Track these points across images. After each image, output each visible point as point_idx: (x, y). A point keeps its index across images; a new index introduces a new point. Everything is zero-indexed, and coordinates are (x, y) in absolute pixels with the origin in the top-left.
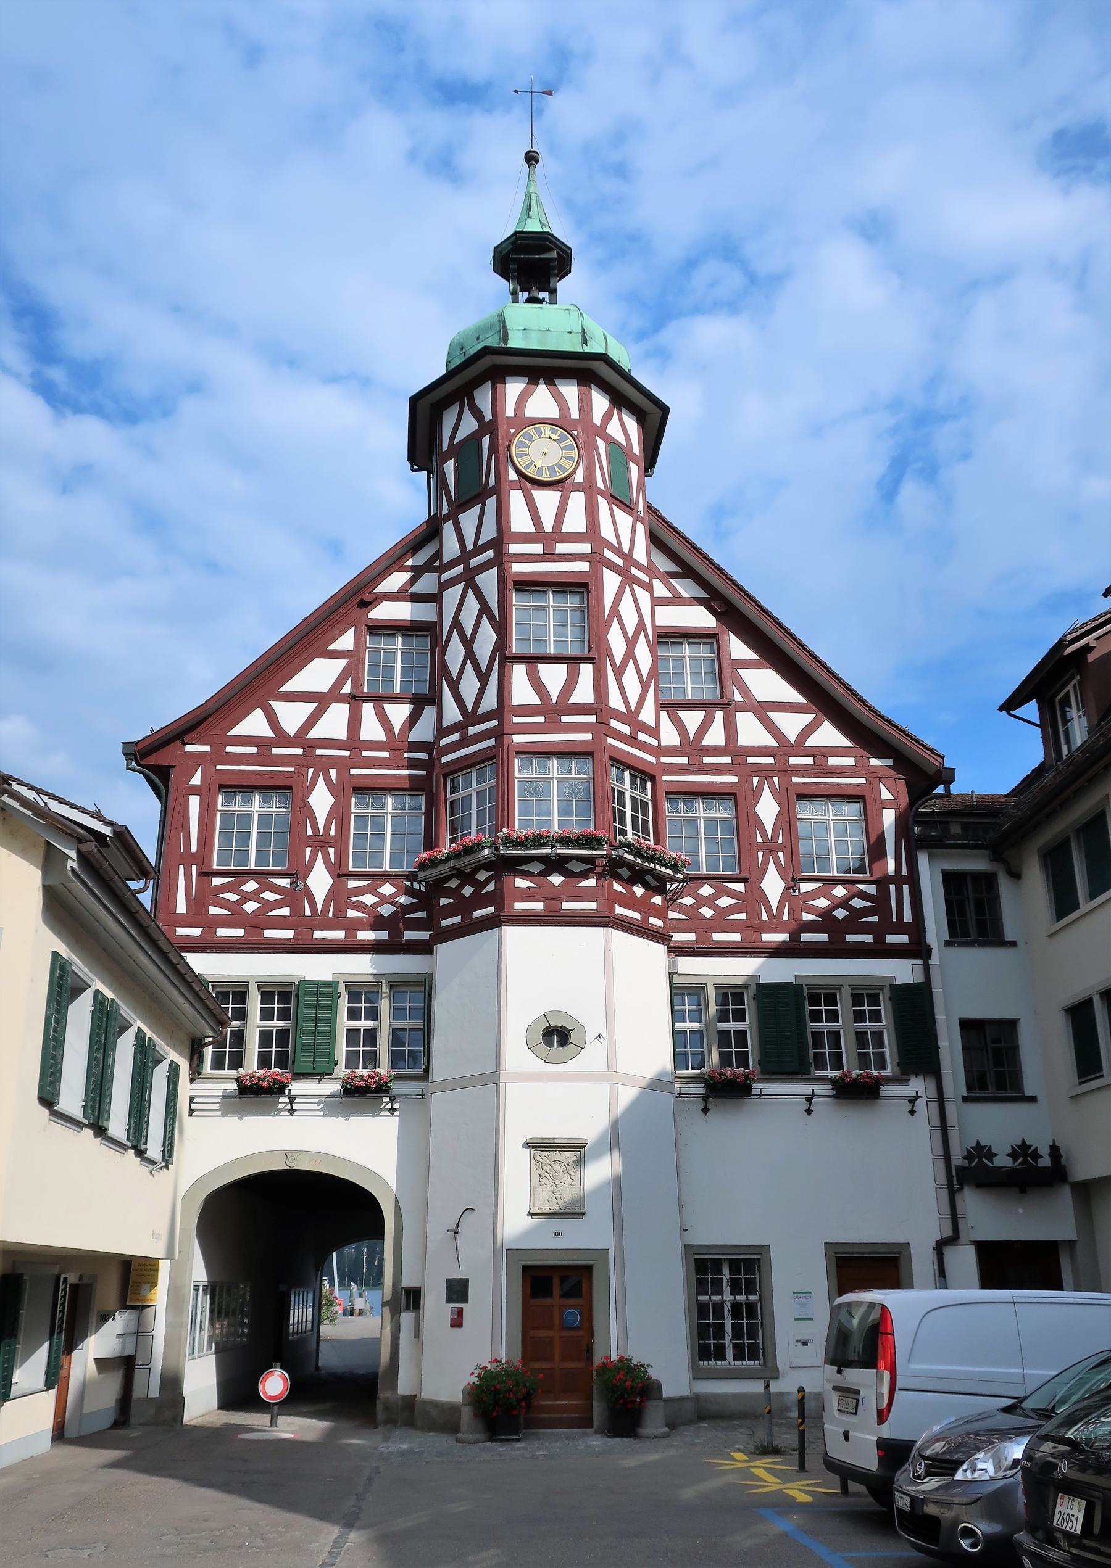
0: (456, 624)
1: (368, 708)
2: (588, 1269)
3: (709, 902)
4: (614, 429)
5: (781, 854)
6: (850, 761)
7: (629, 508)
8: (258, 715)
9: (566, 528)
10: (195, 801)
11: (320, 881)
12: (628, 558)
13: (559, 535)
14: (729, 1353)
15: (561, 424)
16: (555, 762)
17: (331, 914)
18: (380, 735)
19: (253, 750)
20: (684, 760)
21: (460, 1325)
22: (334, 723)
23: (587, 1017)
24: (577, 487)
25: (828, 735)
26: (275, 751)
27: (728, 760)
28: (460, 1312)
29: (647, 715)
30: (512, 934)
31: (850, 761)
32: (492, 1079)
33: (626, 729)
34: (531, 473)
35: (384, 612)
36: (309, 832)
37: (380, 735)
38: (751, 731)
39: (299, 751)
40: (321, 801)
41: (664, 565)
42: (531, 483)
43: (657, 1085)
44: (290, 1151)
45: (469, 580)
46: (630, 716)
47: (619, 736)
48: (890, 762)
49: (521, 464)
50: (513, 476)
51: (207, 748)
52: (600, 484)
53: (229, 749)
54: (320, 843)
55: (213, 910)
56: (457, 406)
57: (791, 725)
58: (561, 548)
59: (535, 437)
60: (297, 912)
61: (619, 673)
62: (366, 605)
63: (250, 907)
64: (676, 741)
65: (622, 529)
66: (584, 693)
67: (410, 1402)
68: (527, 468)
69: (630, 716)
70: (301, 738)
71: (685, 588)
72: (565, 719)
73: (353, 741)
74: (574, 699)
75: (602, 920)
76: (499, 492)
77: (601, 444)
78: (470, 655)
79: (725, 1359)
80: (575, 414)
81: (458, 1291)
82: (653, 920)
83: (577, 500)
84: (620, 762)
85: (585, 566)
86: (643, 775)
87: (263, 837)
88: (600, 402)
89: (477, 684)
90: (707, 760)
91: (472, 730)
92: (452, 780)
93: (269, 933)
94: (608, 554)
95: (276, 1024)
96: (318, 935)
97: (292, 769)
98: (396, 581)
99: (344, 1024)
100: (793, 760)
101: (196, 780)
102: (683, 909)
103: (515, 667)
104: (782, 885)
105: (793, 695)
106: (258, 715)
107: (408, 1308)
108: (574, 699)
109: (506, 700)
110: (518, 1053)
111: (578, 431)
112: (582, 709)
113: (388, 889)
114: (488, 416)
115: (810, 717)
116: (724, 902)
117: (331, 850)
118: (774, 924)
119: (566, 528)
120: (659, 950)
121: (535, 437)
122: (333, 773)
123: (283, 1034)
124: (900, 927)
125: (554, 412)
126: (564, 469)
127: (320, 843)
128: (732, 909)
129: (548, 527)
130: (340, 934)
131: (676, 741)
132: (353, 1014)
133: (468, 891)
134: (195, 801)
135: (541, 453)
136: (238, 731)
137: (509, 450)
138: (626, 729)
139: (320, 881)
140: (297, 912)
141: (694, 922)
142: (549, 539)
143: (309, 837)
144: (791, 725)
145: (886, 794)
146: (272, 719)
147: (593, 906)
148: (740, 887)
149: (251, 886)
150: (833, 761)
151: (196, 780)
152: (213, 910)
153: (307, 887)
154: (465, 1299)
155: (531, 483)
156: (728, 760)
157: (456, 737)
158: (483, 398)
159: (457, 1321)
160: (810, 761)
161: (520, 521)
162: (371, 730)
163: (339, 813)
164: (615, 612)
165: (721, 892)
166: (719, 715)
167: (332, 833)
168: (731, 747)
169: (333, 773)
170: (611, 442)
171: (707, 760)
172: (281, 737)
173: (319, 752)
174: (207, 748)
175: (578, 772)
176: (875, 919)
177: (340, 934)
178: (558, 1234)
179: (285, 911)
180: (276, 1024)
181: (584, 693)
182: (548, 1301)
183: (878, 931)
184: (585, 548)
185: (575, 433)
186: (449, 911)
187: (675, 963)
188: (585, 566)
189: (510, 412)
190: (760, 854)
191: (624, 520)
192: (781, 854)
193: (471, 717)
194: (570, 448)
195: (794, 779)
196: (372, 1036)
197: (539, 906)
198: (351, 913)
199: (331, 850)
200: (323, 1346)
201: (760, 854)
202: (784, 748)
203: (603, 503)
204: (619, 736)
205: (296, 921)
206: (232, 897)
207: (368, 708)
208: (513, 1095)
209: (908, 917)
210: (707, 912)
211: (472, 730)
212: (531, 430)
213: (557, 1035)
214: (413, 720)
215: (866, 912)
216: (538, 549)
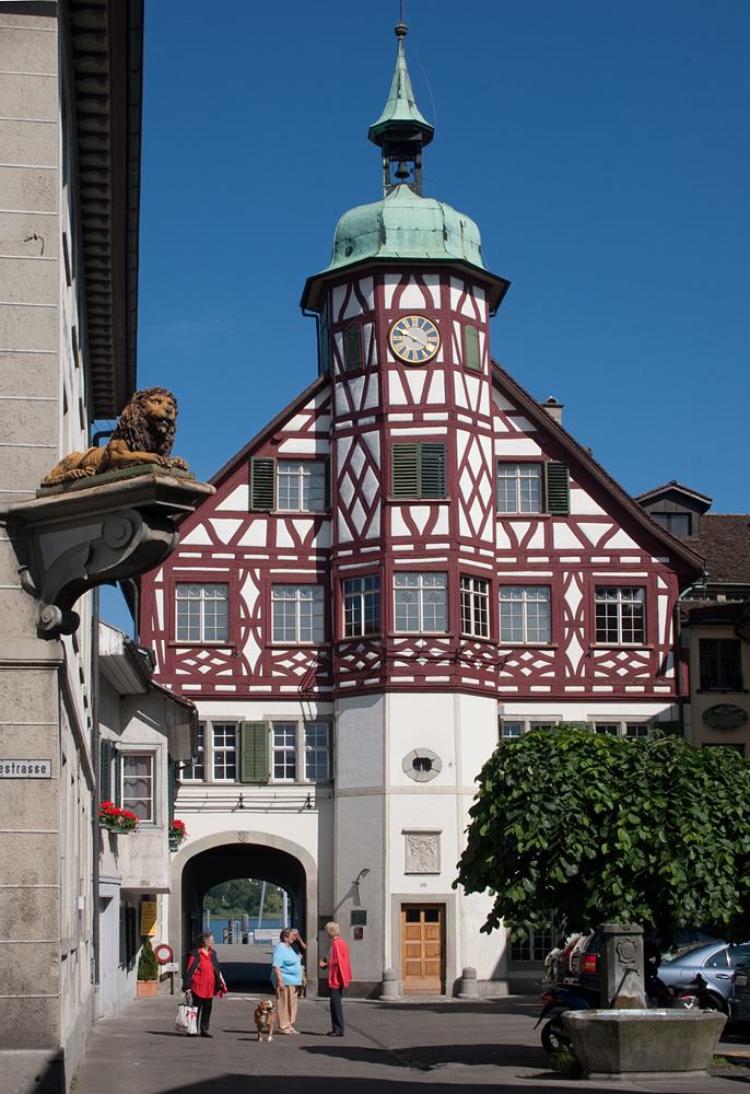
0: (348, 467)
1: (281, 523)
2: (443, 905)
3: (528, 664)
4: (468, 310)
5: (582, 630)
6: (637, 560)
7: (477, 373)
8: (201, 527)
9: (430, 401)
10: (159, 594)
11: (252, 651)
12: (476, 416)
13: (426, 407)
14: (532, 956)
15: (428, 313)
16: (421, 579)
19: (199, 555)
20: (514, 560)
23: (441, 751)
24: (439, 366)
26: (214, 556)
27: (546, 559)
28: (361, 930)
29: (487, 536)
30: (393, 699)
31: (637, 560)
32: (381, 792)
33: (471, 550)
35: (290, 447)
36: (243, 616)
38: (564, 537)
39: (232, 556)
40: (250, 592)
41: (504, 405)
42: (403, 365)
43: (418, 191)
44: (243, 832)
45: (357, 434)
46: (476, 541)
47: (467, 556)
48: (666, 560)
50: (391, 359)
52: (456, 361)
53: (181, 555)
54: (251, 624)
55: (179, 672)
56: (344, 288)
57: (594, 532)
58: (427, 416)
59: (430, 339)
61: (467, 509)
62: (278, 442)
63: (205, 669)
65: (474, 393)
66: (442, 527)
68: (401, 352)
70: (232, 546)
72: (429, 547)
74: (435, 532)
75: (452, 688)
76: (380, 369)
77: (457, 325)
78: (359, 493)
79: (529, 959)
80: (437, 305)
82: (487, 683)
83: (439, 375)
84: (465, 577)
85: (443, 430)
86: (482, 580)
87: (209, 620)
88: (456, 293)
90: (530, 560)
92: (346, 583)
93: (218, 688)
94: (461, 417)
95: (226, 748)
96: (253, 689)
97: (227, 570)
98: (298, 422)
99: (273, 747)
100: (594, 560)
101: (159, 578)
102: (510, 670)
103: (393, 508)
104: (581, 652)
105: (599, 511)
106: (201, 527)
108: (435, 532)
109: (387, 532)
110: (397, 774)
111: (441, 319)
112: (440, 539)
113: (300, 656)
114: (372, 307)
116: (540, 664)
117: (259, 629)
118: (575, 680)
119: (430, 401)
121: (408, 326)
122: (257, 571)
123: (231, 756)
125: (421, 304)
126: (429, 353)
127: (251, 624)
128: (545, 669)
129: (417, 400)
130: (268, 688)
132: (279, 742)
134: (159, 594)
135: (412, 339)
137: (388, 337)
138: (471, 550)
139: (252, 651)
140: (237, 673)
141: (518, 678)
142: (418, 410)
144: (594, 532)
145: (661, 584)
147: (447, 679)
148: (551, 654)
149: (204, 655)
150: (624, 560)
151: (159, 578)
152: (179, 672)
153: (243, 655)
154: (365, 923)
155: (403, 365)
156: (546, 559)
158: (366, 285)
160: (607, 560)
161: (396, 396)
162: (284, 539)
163: (263, 602)
164: (466, 462)
165: (538, 657)
166: (541, 525)
167: (259, 616)
168: (549, 549)
169: (257, 571)
170: (465, 321)
171: (530, 560)
172: (218, 545)
173: (246, 557)
175: (438, 584)
176: (647, 675)
177: (268, 688)
178: (424, 885)
179: (229, 672)
180: (226, 748)
181: (442, 527)
182: (418, 924)
183: (648, 684)
184: (444, 416)
185: (438, 321)
186: (346, 677)
188: (443, 430)
189: (388, 305)
190: (567, 629)
191: (473, 382)
192: (582, 630)
194: (433, 334)
195: (594, 574)
196: (292, 758)
197: (411, 679)
198: (275, 674)
199: (259, 629)
201: (567, 629)
202: (589, 550)
203: (457, 375)
204: (467, 556)
205: (235, 678)
206: (191, 662)
207: (281, 523)
208: (393, 802)
210: (526, 672)
212: (404, 321)
213: (423, 764)
214: (316, 530)
215: (641, 670)
216: (409, 417)
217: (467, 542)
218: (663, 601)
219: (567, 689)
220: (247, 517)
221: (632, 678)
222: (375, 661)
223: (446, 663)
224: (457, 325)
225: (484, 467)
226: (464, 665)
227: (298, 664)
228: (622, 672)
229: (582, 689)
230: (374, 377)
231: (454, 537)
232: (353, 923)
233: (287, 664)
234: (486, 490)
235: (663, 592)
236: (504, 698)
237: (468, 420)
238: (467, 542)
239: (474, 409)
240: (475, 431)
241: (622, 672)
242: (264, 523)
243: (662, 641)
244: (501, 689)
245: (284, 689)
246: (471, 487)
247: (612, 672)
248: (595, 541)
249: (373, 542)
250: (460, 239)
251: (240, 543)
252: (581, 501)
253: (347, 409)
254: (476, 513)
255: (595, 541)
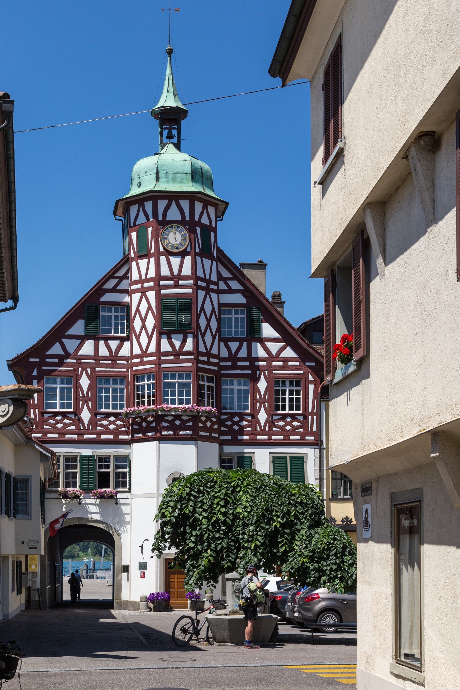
1: (102, 343)
5: (266, 404)
8: (57, 345)
9: (184, 273)
12: (209, 282)
13: (180, 277)
17: (91, 429)
18: (107, 354)
19: (56, 360)
20: (230, 364)
21: (144, 577)
22: (88, 348)
25: (289, 353)
27: (247, 364)
28: (144, 573)
33: (205, 359)
34: (169, 248)
37: (107, 354)
41: (225, 274)
45: (143, 291)
46: (208, 354)
49: (166, 242)
51: (38, 360)
53: (47, 360)
57: (274, 347)
58: (181, 282)
60: (78, 428)
61: (203, 335)
63: (60, 426)
64: (227, 356)
67: (127, 602)
69: (208, 354)
71: (235, 285)
72: (182, 357)
73: (96, 356)
74: (185, 349)
77: (198, 229)
80: (187, 218)
81: (143, 566)
83: (188, 259)
85: (190, 290)
89: (140, 308)
90: (239, 364)
91: (145, 359)
98: (111, 284)
101: (35, 373)
105: (276, 335)
106: (57, 345)
107: (124, 572)
108: (185, 349)
115: (283, 344)
118: (262, 433)
120: (216, 446)
124: (311, 433)
129: (176, 272)
131: (227, 356)
133: (144, 424)
136: (50, 352)
138: (205, 359)
142: (176, 278)
143: (81, 397)
144: (274, 347)
146: (63, 347)
151: (35, 373)
156: (247, 364)
157: (138, 360)
159: (143, 576)
160: (281, 363)
161: (165, 271)
162: (103, 351)
166: (245, 344)
170: (203, 227)
171: (239, 364)
174: (38, 360)
176: (302, 430)
179: (73, 427)
185: (188, 227)
187: (222, 448)
188: (190, 290)
191: (207, 262)
193: (145, 353)
198: (98, 428)
200: (390, 541)
202: (271, 358)
203: (198, 258)
207: (102, 343)
209: (315, 429)
210: (236, 428)
211: (145, 359)
217: (203, 354)
218: (311, 388)
219: (258, 437)
220: (83, 339)
221: (294, 431)
222: (152, 422)
223: (191, 424)
224: (198, 229)
225: (213, 311)
226: (200, 425)
227: (111, 423)
228: (288, 428)
229: (266, 437)
230: (152, 260)
231: (196, 353)
232: (140, 569)
233: (105, 422)
234: (214, 324)
235: (311, 382)
236: (222, 443)
237: (204, 285)
238: (203, 354)
239: (208, 278)
240: (208, 291)
241: (288, 428)
242: (92, 342)
243: (310, 410)
244: (221, 438)
245: (103, 437)
246: (206, 323)
247: (282, 428)
248: (274, 352)
249: (151, 355)
250: (201, 178)
251: (80, 353)
252: (268, 330)
253: (138, 278)
254: (208, 338)
255: (274, 352)
